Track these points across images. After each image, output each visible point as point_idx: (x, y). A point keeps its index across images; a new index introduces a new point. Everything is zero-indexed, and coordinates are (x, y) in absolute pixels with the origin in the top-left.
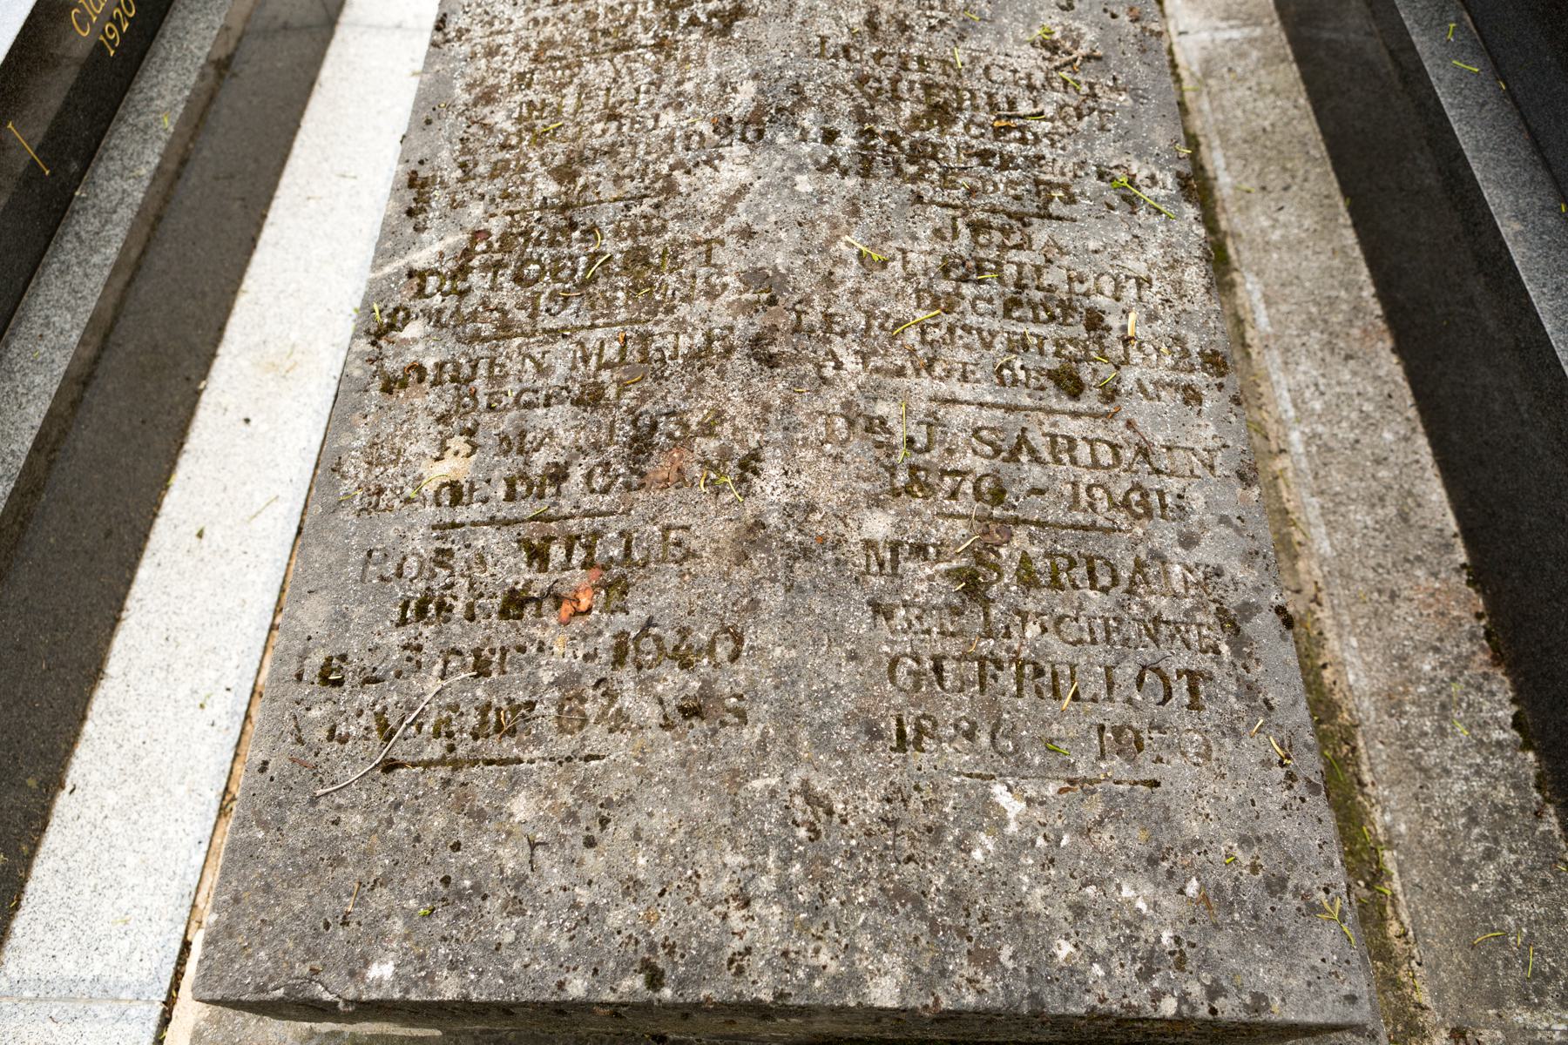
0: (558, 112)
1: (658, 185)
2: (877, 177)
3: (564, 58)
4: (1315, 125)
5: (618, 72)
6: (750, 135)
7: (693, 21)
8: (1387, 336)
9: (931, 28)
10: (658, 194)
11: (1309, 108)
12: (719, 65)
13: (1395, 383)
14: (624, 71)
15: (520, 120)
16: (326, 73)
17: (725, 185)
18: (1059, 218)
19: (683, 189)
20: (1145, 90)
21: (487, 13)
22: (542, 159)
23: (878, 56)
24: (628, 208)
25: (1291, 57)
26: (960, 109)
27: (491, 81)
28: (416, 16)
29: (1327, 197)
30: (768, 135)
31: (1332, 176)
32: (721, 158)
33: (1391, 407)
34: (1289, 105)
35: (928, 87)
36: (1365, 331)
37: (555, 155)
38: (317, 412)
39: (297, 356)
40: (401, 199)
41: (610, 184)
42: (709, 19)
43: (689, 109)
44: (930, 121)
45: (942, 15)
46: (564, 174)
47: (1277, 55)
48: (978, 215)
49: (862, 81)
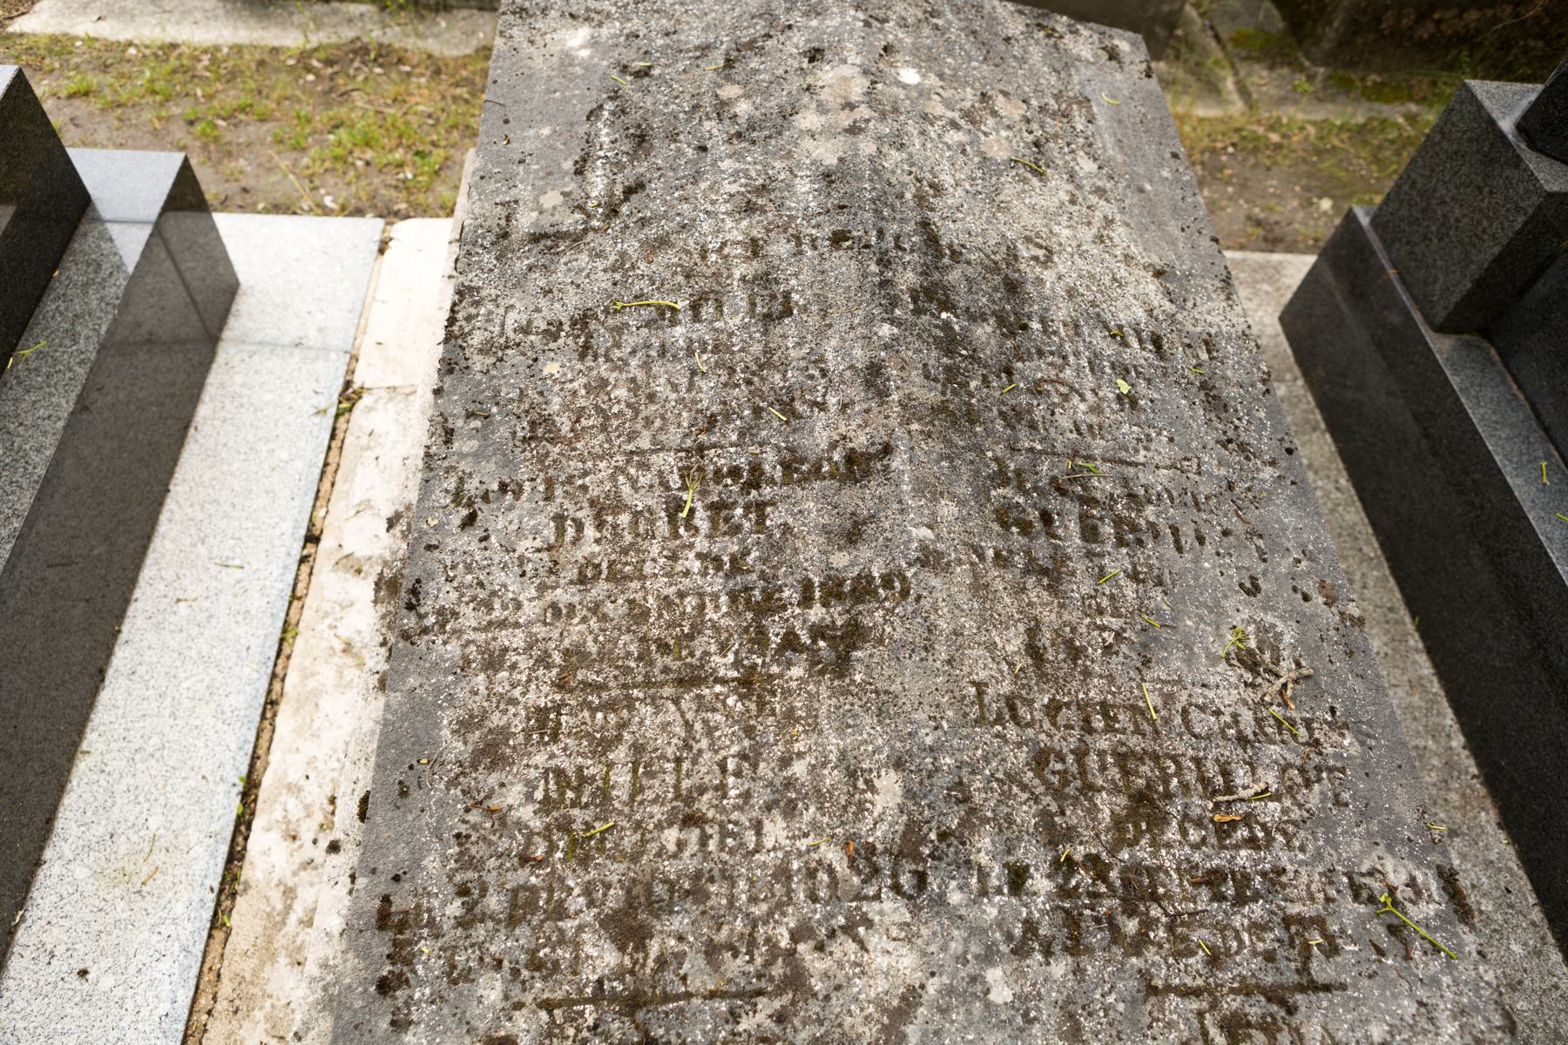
0: (604, 795)
1: (778, 970)
2: (1089, 951)
3: (603, 687)
4: (1363, 515)
5: (688, 726)
6: (905, 880)
7: (790, 642)
8: (1488, 803)
9: (1108, 650)
10: (779, 991)
11: (1353, 492)
12: (840, 731)
13: (1510, 870)
14: (698, 726)
15: (547, 805)
16: (203, 411)
17: (881, 985)
18: (1327, 988)
19: (818, 986)
20: (1369, 723)
21: (481, 584)
22: (588, 891)
23: (1053, 709)
24: (734, 1016)
25: (1323, 426)
26: (1168, 796)
27: (496, 720)
28: (320, 330)
29: (1391, 609)
30: (934, 885)
31: (1392, 581)
32: (869, 924)
33: (1511, 906)
34: (1330, 487)
35: (1124, 758)
36: (1463, 796)
37: (608, 886)
38: (185, 950)
39: (159, 858)
40: (364, 953)
41: (701, 961)
42: (814, 642)
43: (807, 817)
44: (1137, 826)
45: (1116, 623)
46: (627, 929)
47: (1308, 422)
48: (1231, 1003)
49: (1040, 759)
